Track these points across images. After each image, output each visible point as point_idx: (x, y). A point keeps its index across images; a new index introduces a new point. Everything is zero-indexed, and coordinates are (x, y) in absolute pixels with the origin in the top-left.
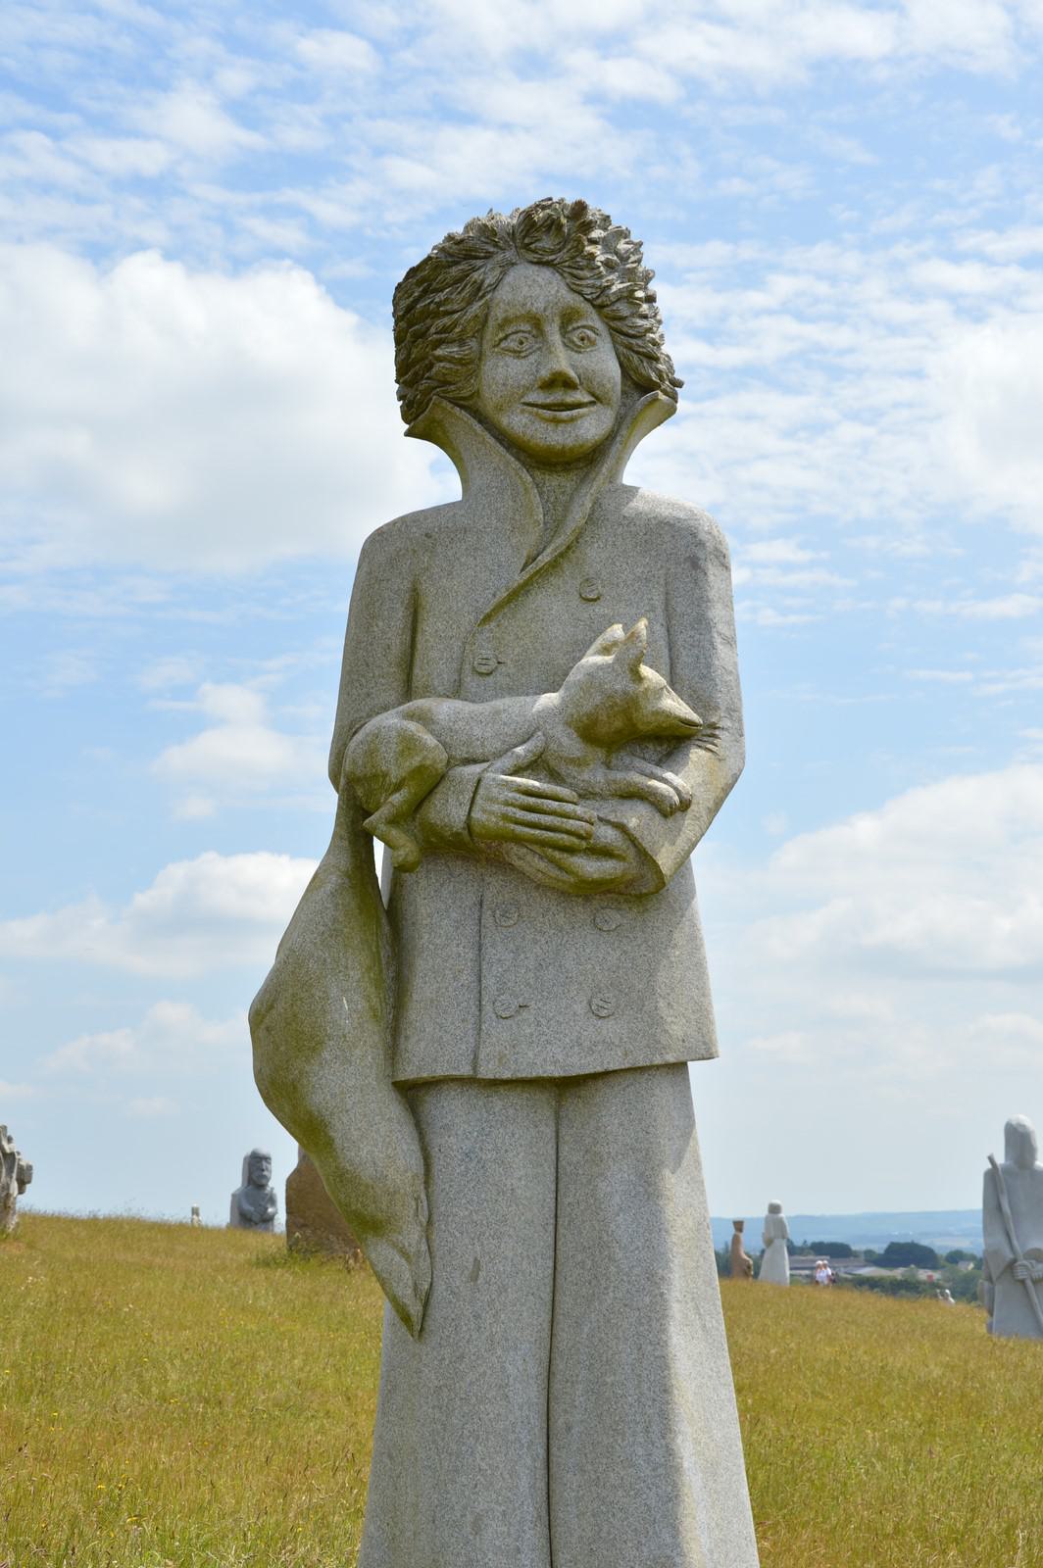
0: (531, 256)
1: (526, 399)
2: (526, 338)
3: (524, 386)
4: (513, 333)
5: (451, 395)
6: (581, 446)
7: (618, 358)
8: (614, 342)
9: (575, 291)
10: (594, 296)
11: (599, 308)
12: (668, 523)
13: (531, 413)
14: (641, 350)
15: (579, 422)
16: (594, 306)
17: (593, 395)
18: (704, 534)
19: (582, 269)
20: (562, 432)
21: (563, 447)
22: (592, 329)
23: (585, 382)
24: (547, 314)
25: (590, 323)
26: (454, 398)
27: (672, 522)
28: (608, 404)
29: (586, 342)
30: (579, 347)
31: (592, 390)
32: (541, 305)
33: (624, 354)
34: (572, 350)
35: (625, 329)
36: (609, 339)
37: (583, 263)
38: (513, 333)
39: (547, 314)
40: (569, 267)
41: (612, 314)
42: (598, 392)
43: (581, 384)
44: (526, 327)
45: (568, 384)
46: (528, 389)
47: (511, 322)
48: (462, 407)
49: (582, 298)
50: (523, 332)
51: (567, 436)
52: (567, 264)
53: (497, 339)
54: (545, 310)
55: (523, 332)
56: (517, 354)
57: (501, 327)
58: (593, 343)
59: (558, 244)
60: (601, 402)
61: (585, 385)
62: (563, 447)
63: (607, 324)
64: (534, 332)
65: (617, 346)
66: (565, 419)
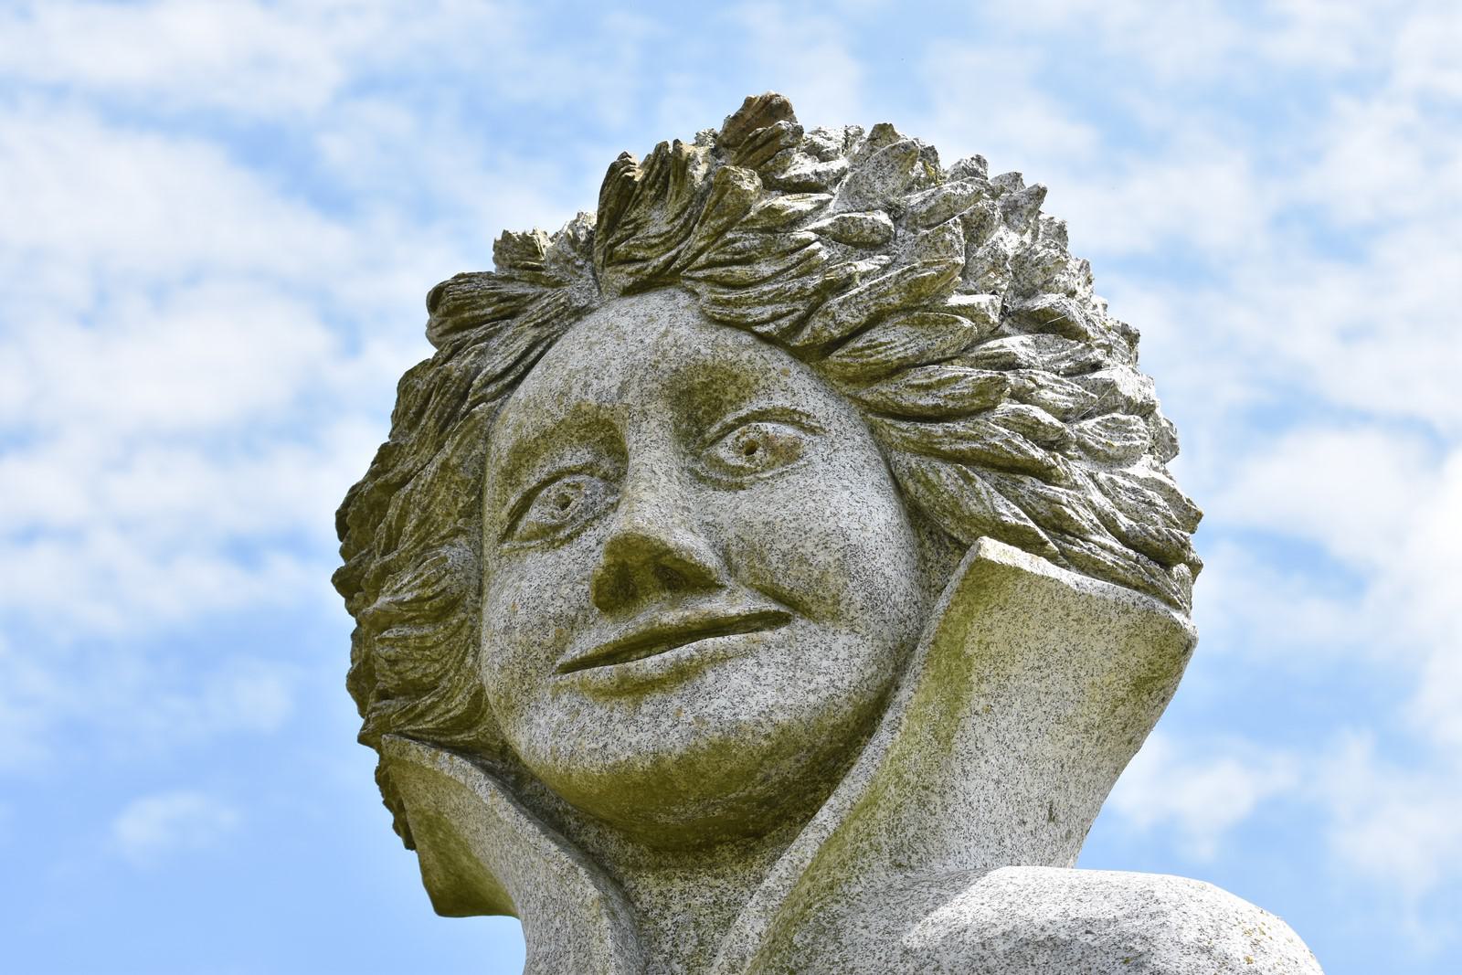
0: (622, 277)
1: (573, 653)
2: (577, 486)
3: (558, 619)
4: (544, 484)
5: (426, 724)
6: (721, 749)
7: (900, 490)
8: (884, 449)
9: (722, 323)
10: (784, 323)
11: (814, 355)
12: (1053, 944)
13: (570, 688)
14: (964, 446)
15: (711, 677)
16: (799, 355)
17: (777, 597)
18: (1175, 954)
19: (748, 261)
20: (655, 718)
21: (657, 761)
22: (787, 416)
23: (743, 562)
24: (628, 400)
25: (780, 401)
26: (438, 731)
27: (1063, 935)
28: (836, 616)
29: (759, 454)
30: (738, 471)
31: (767, 583)
32: (611, 383)
33: (912, 474)
34: (717, 485)
35: (911, 400)
36: (859, 437)
37: (751, 241)
38: (544, 484)
39: (628, 400)
40: (711, 264)
41: (854, 366)
42: (786, 585)
43: (733, 570)
44: (575, 457)
45: (680, 577)
46: (572, 624)
47: (536, 456)
48: (457, 749)
49: (746, 339)
50: (571, 472)
51: (666, 723)
52: (702, 259)
53: (504, 513)
54: (623, 390)
55: (571, 472)
56: (549, 536)
57: (510, 475)
58: (789, 454)
59: (677, 216)
60: (807, 613)
61: (744, 573)
62: (657, 761)
63: (855, 399)
64: (606, 465)
65: (895, 456)
66: (657, 673)
